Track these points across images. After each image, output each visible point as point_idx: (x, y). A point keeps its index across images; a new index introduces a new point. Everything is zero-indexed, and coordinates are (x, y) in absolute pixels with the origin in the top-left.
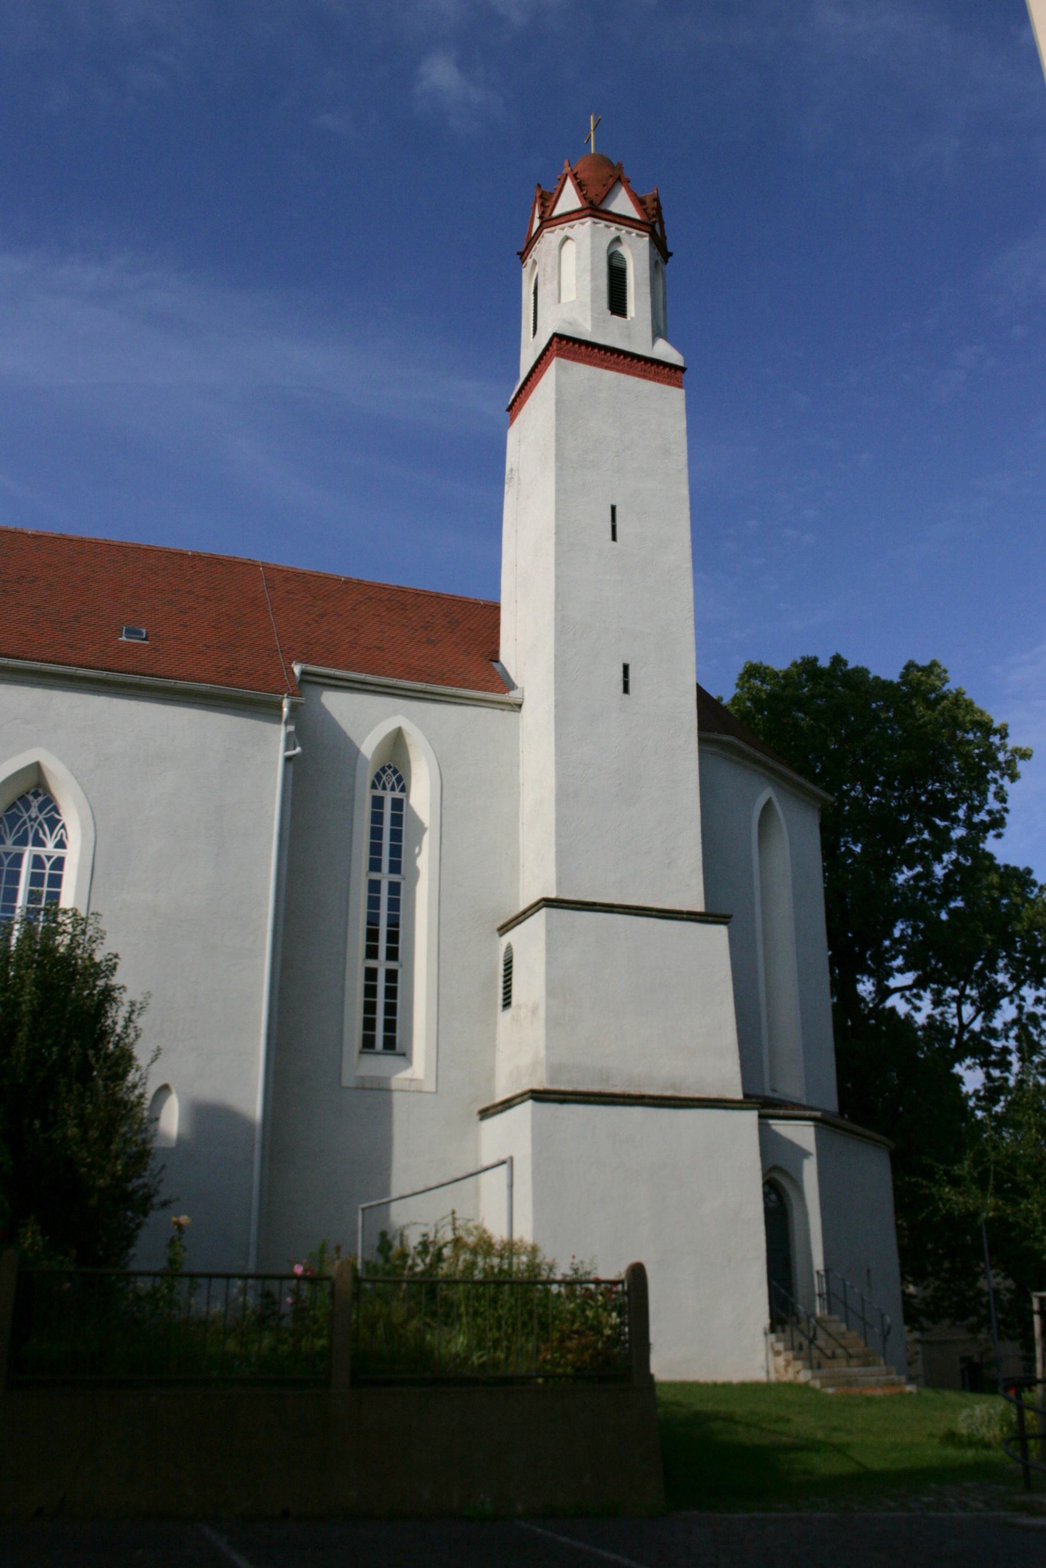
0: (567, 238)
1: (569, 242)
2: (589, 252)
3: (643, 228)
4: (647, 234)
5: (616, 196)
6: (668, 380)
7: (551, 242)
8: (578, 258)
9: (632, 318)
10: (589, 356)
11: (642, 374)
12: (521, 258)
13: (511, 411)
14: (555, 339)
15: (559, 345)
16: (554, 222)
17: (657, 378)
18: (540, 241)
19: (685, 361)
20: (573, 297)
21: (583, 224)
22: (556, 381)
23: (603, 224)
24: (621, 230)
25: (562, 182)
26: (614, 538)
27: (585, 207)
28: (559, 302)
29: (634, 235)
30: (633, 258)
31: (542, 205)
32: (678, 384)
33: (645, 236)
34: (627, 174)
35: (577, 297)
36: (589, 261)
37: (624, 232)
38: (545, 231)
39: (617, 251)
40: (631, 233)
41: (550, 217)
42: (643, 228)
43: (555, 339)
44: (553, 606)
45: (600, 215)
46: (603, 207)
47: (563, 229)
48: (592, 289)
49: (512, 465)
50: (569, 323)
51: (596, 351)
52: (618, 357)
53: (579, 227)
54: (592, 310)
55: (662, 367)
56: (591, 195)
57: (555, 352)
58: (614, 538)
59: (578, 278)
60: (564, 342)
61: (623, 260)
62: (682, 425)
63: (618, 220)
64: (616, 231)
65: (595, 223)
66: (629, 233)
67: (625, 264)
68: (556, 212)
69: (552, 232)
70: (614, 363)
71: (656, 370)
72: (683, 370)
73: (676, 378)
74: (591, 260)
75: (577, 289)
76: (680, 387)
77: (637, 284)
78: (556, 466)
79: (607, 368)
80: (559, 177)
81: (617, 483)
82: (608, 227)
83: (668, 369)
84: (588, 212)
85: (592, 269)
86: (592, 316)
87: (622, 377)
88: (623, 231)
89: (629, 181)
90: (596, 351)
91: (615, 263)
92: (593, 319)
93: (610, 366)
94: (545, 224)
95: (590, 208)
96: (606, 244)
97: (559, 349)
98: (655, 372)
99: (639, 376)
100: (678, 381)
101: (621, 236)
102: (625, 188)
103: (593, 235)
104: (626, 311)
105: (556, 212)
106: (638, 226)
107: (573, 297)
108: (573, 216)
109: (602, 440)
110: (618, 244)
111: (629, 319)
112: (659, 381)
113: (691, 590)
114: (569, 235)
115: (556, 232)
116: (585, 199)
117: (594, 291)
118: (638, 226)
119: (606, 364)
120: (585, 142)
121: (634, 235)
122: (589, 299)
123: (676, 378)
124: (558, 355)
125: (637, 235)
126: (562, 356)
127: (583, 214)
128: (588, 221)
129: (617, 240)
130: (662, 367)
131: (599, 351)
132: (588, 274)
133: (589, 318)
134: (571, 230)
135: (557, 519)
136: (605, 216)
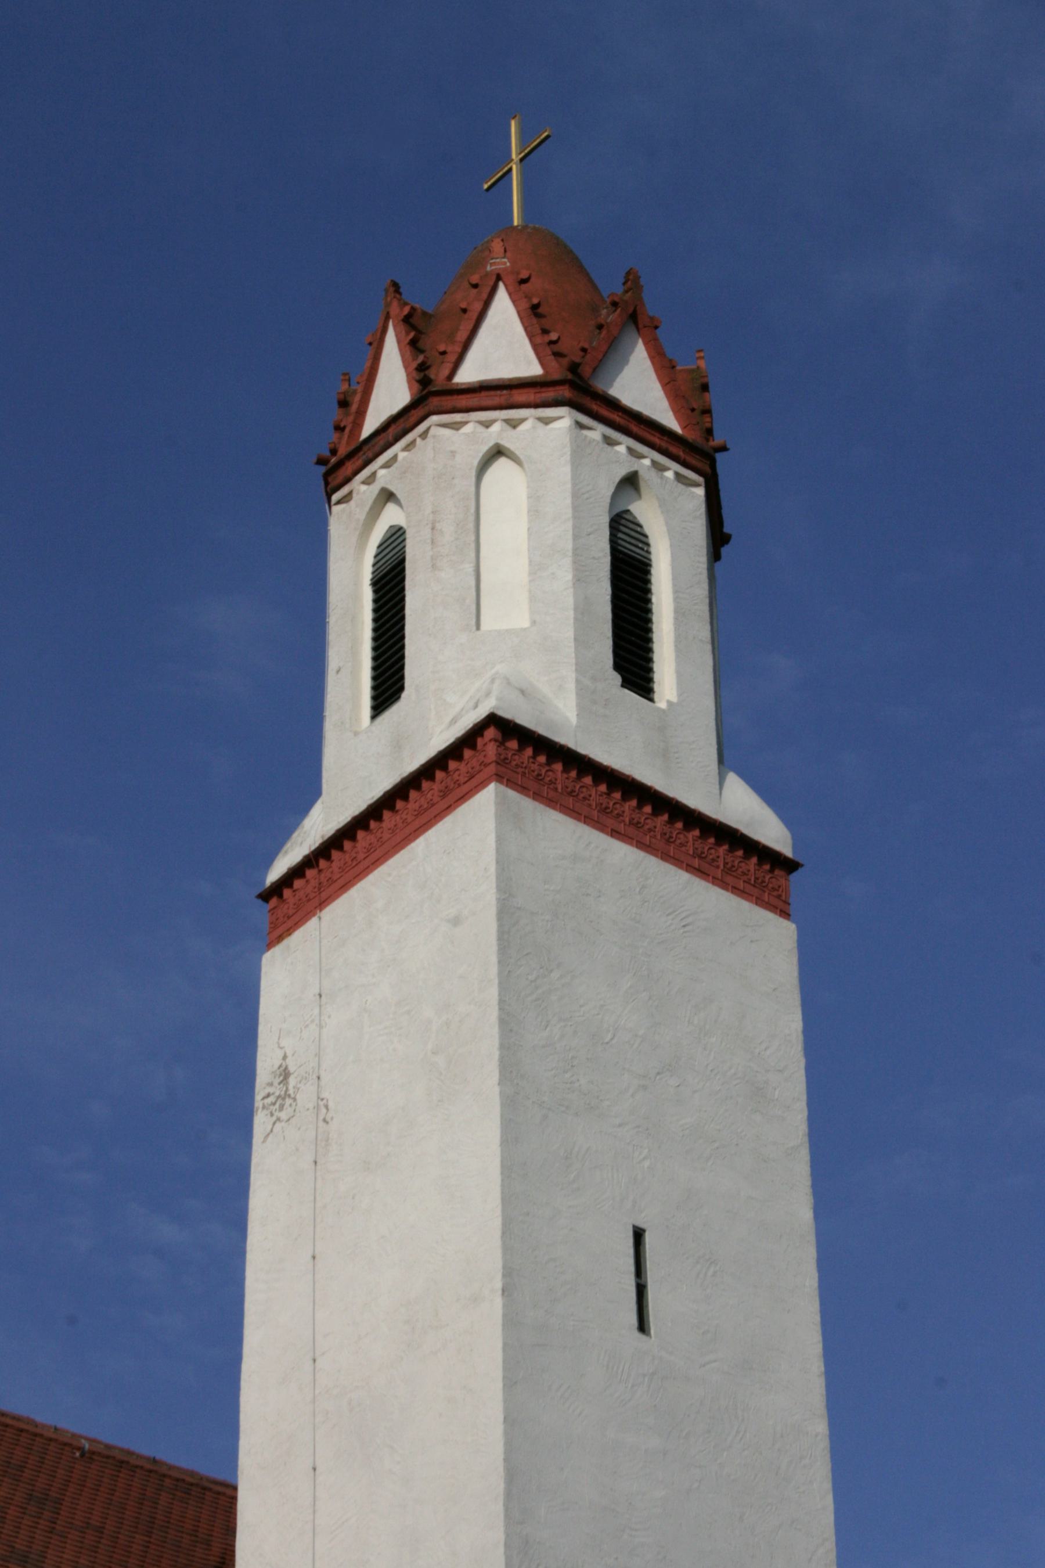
0: (498, 452)
1: (502, 462)
2: (569, 501)
3: (694, 462)
4: (700, 479)
5: (625, 361)
6: (756, 892)
7: (453, 453)
8: (534, 513)
9: (669, 703)
10: (570, 794)
11: (696, 862)
12: (326, 476)
13: (274, 901)
14: (491, 733)
15: (501, 750)
16: (463, 401)
17: (729, 879)
18: (413, 443)
19: (797, 842)
20: (521, 620)
21: (546, 421)
22: (498, 850)
23: (597, 432)
24: (642, 457)
25: (485, 296)
26: (643, 1326)
27: (556, 376)
28: (478, 626)
29: (670, 474)
30: (671, 538)
31: (413, 346)
32: (780, 904)
33: (696, 485)
34: (652, 305)
35: (534, 623)
36: (569, 525)
37: (647, 462)
38: (434, 419)
39: (628, 511)
40: (666, 469)
41: (448, 387)
42: (694, 462)
43: (491, 733)
44: (499, 1507)
45: (594, 407)
46: (599, 385)
47: (487, 424)
48: (576, 609)
49: (285, 1057)
50: (523, 692)
51: (588, 780)
52: (640, 806)
53: (534, 428)
54: (580, 669)
55: (740, 853)
56: (570, 346)
57: (492, 768)
58: (643, 1326)
59: (536, 569)
60: (513, 744)
61: (642, 539)
62: (793, 1023)
63: (634, 428)
64: (630, 458)
65: (580, 426)
66: (659, 468)
67: (649, 552)
68: (468, 374)
69: (456, 426)
70: (631, 823)
71: (729, 859)
72: (790, 866)
73: (774, 889)
74: (575, 527)
75: (532, 599)
76: (785, 914)
77: (680, 614)
78: (502, 1093)
79: (615, 833)
80: (475, 279)
81: (647, 1164)
82: (609, 442)
83: (754, 860)
84: (566, 392)
85: (576, 552)
86: (578, 681)
87: (652, 863)
88: (647, 461)
89: (656, 327)
90: (588, 780)
91: (627, 547)
92: (581, 690)
93: (621, 828)
94: (435, 402)
95: (572, 384)
96: (606, 488)
97: (502, 761)
98: (726, 864)
99: (690, 868)
100: (779, 897)
101: (641, 473)
102: (646, 344)
103: (578, 454)
104: (650, 680)
105: (468, 374)
106: (681, 454)
107: (521, 620)
108: (520, 396)
109: (610, 1036)
110: (630, 491)
111: (661, 704)
112: (736, 890)
113: (829, 1500)
114: (506, 443)
115: (467, 429)
116: (557, 355)
117: (583, 611)
118: (681, 454)
119: (610, 822)
120: (486, 186)
121: (670, 474)
122: (570, 633)
123: (774, 889)
124: (499, 778)
125: (678, 476)
126: (511, 783)
127: (550, 394)
128: (564, 419)
129: (631, 482)
130: (740, 853)
131: (596, 782)
132: (567, 562)
133: (571, 686)
134: (510, 432)
135: (507, 1249)
136: (604, 412)
